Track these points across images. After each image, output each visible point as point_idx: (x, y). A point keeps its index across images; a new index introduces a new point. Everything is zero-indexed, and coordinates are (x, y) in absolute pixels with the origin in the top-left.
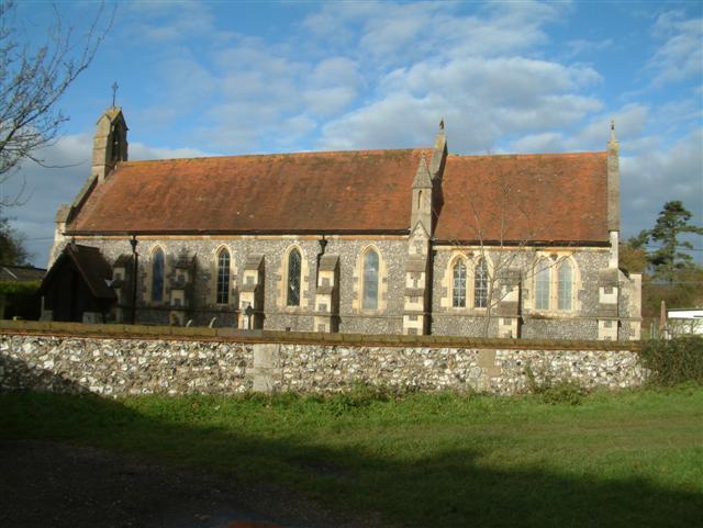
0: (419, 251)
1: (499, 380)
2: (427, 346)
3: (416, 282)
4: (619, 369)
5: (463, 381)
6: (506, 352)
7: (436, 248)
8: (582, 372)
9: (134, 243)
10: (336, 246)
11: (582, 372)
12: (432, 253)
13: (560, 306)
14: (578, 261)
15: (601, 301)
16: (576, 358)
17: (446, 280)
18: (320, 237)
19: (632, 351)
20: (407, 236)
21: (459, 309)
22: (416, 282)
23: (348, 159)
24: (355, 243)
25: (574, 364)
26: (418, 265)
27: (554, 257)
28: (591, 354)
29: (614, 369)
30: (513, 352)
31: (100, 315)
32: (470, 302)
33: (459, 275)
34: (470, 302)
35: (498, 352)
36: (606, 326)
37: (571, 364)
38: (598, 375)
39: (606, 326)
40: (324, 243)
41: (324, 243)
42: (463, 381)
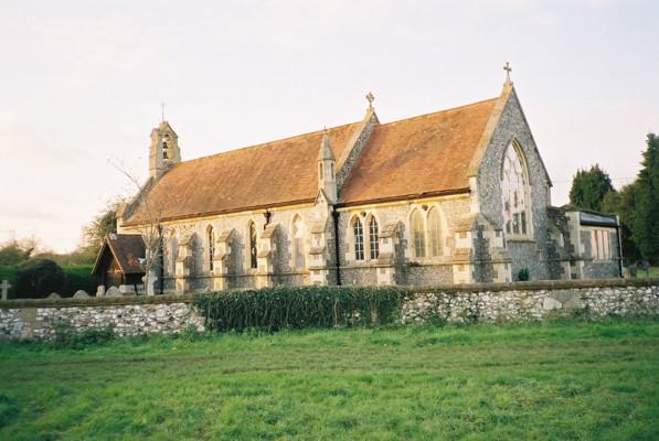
0: (321, 214)
1: (42, 330)
2: (650, 286)
3: (318, 243)
4: (171, 319)
5: (8, 333)
6: (47, 310)
7: (338, 210)
8: (128, 322)
9: (160, 229)
10: (281, 217)
11: (128, 322)
12: (336, 216)
13: (435, 254)
14: (444, 210)
15: (458, 246)
16: (120, 311)
17: (348, 237)
18: (265, 211)
19: (187, 303)
20: (467, 195)
21: (359, 261)
22: (318, 243)
23: (305, 141)
24: (286, 212)
25: (120, 316)
26: (319, 227)
27: (425, 208)
28: (137, 307)
29: (167, 319)
30: (54, 309)
31: (133, 287)
32: (367, 255)
33: (358, 231)
34: (367, 255)
35: (40, 310)
36: (460, 270)
37: (114, 316)
38: (147, 325)
39: (460, 270)
40: (268, 215)
41: (268, 215)
42: (8, 333)
